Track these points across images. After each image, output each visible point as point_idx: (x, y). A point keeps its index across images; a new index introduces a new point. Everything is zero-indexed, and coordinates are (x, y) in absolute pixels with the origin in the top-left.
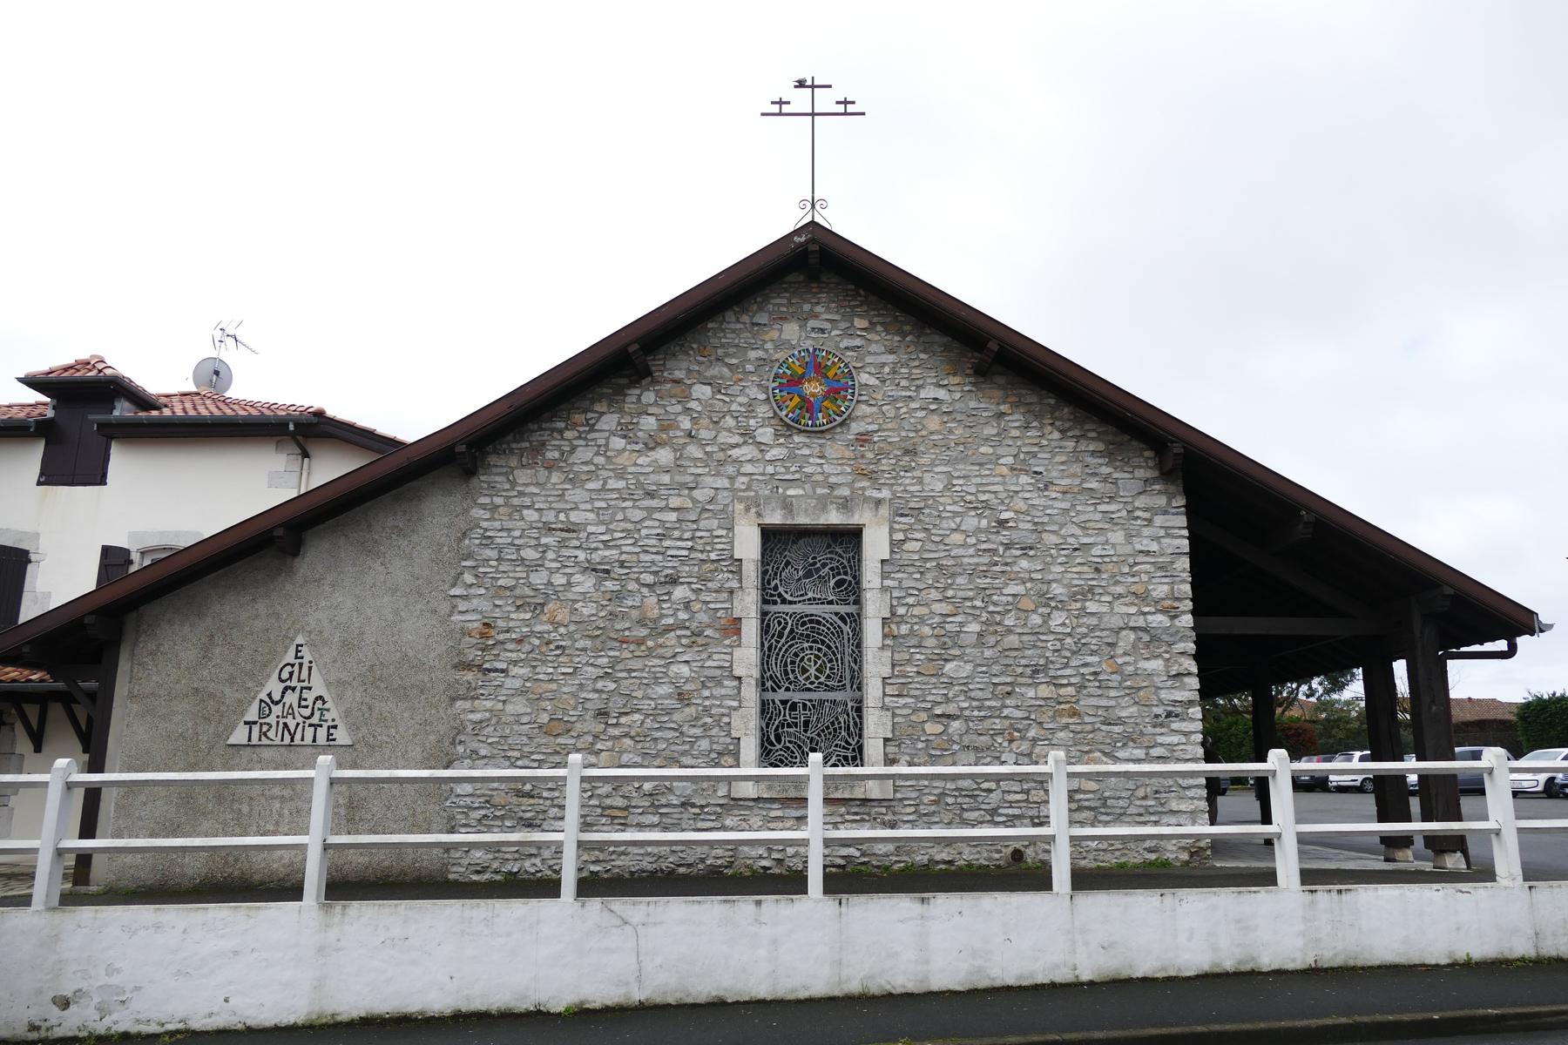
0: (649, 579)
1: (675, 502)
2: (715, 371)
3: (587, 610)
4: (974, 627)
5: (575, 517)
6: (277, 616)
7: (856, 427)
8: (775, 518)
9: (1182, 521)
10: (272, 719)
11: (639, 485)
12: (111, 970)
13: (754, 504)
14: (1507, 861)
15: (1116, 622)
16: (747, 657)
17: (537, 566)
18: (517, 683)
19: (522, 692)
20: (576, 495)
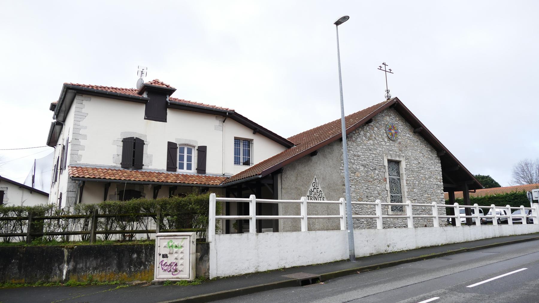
0: (372, 168)
1: (374, 152)
2: (377, 125)
3: (363, 174)
4: (417, 183)
5: (359, 153)
6: (310, 170)
7: (399, 141)
8: (390, 158)
9: (440, 165)
10: (312, 195)
11: (369, 148)
12: (393, 240)
13: (386, 154)
14: (478, 222)
15: (434, 183)
16: (388, 186)
17: (354, 164)
18: (353, 189)
19: (354, 191)
20: (359, 149)
